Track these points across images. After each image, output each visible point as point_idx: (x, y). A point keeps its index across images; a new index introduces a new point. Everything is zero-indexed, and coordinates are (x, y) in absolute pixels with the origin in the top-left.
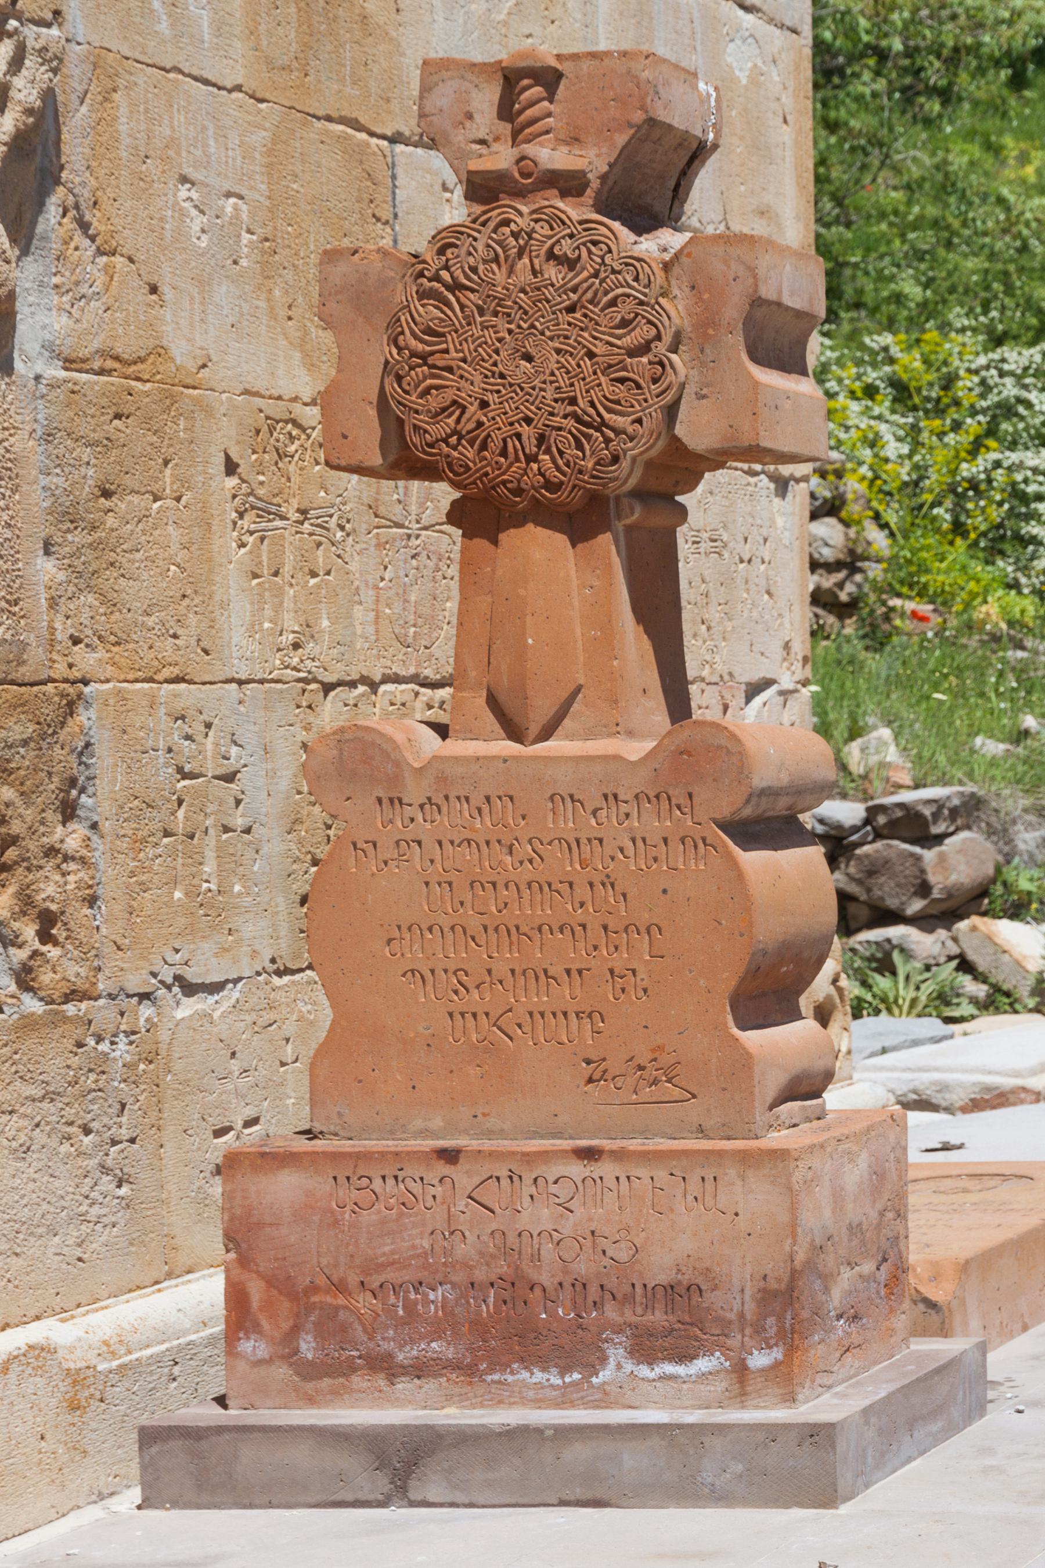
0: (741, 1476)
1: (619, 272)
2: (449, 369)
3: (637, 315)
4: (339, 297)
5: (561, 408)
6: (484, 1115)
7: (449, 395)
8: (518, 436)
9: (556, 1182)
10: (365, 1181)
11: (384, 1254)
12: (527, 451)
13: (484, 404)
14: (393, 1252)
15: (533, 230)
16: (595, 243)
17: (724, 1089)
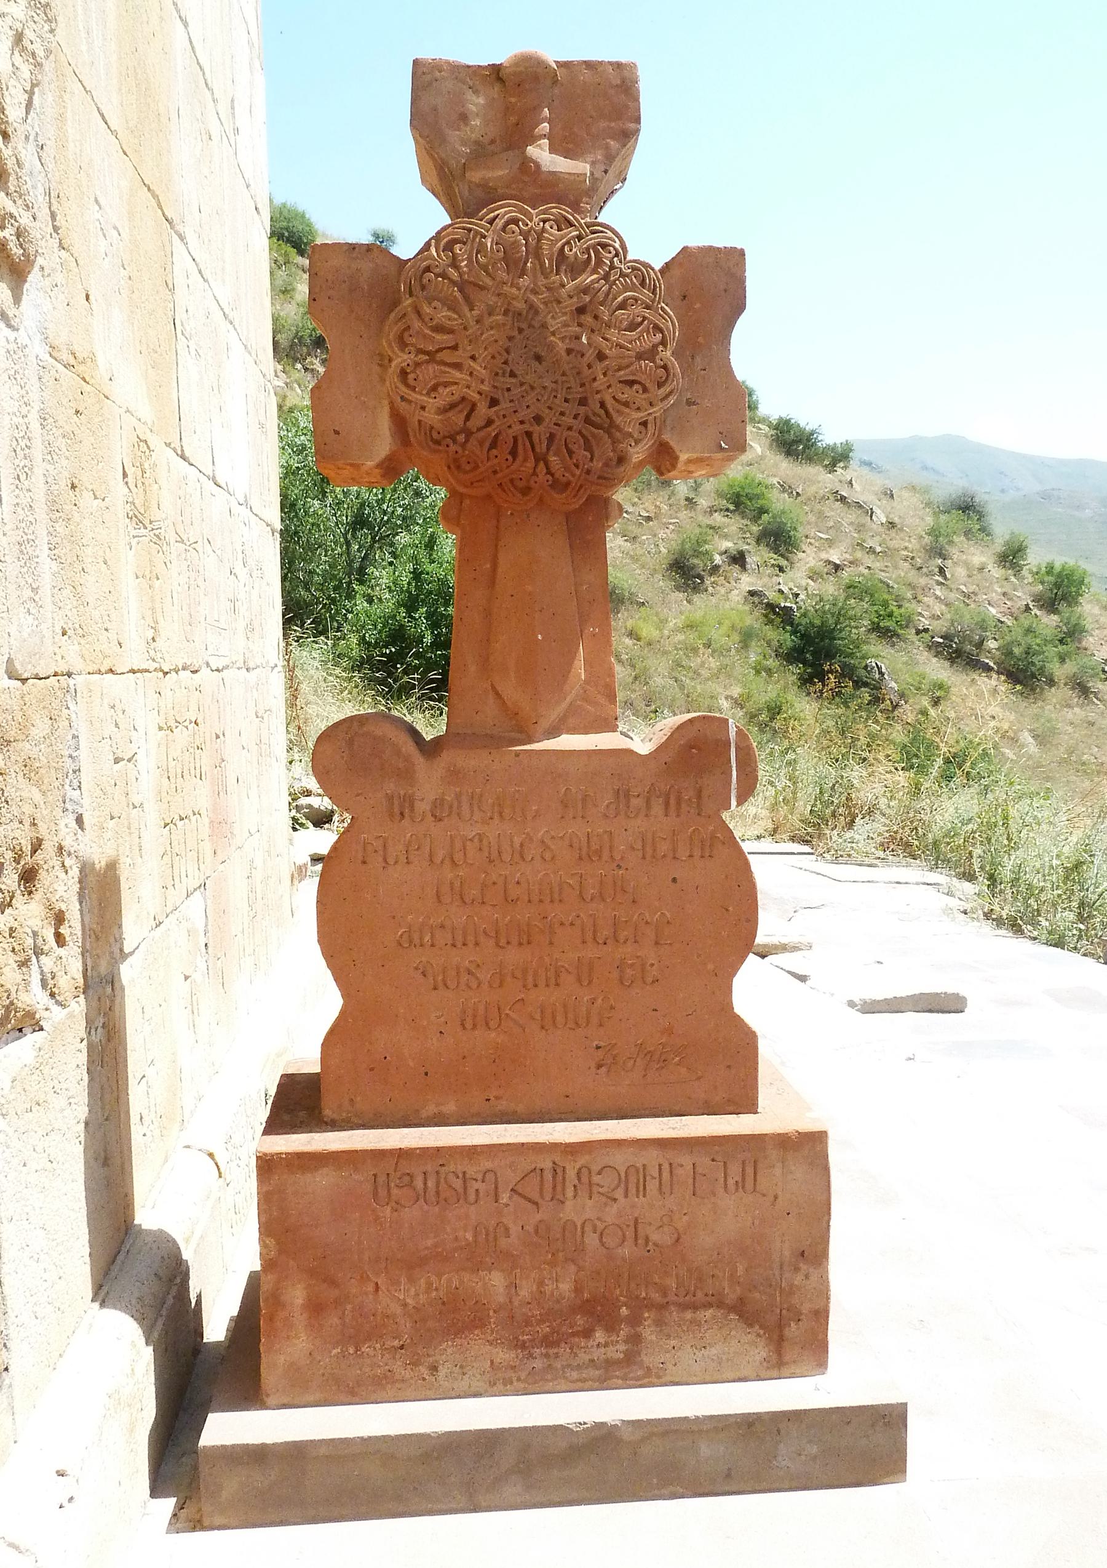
0: (816, 1457)
1: (627, 275)
2: (457, 366)
3: (644, 318)
4: (331, 292)
5: (571, 408)
6: (497, 1098)
7: (458, 392)
8: (529, 434)
9: (599, 1173)
10: (406, 1179)
11: (427, 1248)
12: (538, 450)
13: (494, 402)
14: (436, 1246)
15: (543, 230)
16: (604, 246)
17: (729, 1067)
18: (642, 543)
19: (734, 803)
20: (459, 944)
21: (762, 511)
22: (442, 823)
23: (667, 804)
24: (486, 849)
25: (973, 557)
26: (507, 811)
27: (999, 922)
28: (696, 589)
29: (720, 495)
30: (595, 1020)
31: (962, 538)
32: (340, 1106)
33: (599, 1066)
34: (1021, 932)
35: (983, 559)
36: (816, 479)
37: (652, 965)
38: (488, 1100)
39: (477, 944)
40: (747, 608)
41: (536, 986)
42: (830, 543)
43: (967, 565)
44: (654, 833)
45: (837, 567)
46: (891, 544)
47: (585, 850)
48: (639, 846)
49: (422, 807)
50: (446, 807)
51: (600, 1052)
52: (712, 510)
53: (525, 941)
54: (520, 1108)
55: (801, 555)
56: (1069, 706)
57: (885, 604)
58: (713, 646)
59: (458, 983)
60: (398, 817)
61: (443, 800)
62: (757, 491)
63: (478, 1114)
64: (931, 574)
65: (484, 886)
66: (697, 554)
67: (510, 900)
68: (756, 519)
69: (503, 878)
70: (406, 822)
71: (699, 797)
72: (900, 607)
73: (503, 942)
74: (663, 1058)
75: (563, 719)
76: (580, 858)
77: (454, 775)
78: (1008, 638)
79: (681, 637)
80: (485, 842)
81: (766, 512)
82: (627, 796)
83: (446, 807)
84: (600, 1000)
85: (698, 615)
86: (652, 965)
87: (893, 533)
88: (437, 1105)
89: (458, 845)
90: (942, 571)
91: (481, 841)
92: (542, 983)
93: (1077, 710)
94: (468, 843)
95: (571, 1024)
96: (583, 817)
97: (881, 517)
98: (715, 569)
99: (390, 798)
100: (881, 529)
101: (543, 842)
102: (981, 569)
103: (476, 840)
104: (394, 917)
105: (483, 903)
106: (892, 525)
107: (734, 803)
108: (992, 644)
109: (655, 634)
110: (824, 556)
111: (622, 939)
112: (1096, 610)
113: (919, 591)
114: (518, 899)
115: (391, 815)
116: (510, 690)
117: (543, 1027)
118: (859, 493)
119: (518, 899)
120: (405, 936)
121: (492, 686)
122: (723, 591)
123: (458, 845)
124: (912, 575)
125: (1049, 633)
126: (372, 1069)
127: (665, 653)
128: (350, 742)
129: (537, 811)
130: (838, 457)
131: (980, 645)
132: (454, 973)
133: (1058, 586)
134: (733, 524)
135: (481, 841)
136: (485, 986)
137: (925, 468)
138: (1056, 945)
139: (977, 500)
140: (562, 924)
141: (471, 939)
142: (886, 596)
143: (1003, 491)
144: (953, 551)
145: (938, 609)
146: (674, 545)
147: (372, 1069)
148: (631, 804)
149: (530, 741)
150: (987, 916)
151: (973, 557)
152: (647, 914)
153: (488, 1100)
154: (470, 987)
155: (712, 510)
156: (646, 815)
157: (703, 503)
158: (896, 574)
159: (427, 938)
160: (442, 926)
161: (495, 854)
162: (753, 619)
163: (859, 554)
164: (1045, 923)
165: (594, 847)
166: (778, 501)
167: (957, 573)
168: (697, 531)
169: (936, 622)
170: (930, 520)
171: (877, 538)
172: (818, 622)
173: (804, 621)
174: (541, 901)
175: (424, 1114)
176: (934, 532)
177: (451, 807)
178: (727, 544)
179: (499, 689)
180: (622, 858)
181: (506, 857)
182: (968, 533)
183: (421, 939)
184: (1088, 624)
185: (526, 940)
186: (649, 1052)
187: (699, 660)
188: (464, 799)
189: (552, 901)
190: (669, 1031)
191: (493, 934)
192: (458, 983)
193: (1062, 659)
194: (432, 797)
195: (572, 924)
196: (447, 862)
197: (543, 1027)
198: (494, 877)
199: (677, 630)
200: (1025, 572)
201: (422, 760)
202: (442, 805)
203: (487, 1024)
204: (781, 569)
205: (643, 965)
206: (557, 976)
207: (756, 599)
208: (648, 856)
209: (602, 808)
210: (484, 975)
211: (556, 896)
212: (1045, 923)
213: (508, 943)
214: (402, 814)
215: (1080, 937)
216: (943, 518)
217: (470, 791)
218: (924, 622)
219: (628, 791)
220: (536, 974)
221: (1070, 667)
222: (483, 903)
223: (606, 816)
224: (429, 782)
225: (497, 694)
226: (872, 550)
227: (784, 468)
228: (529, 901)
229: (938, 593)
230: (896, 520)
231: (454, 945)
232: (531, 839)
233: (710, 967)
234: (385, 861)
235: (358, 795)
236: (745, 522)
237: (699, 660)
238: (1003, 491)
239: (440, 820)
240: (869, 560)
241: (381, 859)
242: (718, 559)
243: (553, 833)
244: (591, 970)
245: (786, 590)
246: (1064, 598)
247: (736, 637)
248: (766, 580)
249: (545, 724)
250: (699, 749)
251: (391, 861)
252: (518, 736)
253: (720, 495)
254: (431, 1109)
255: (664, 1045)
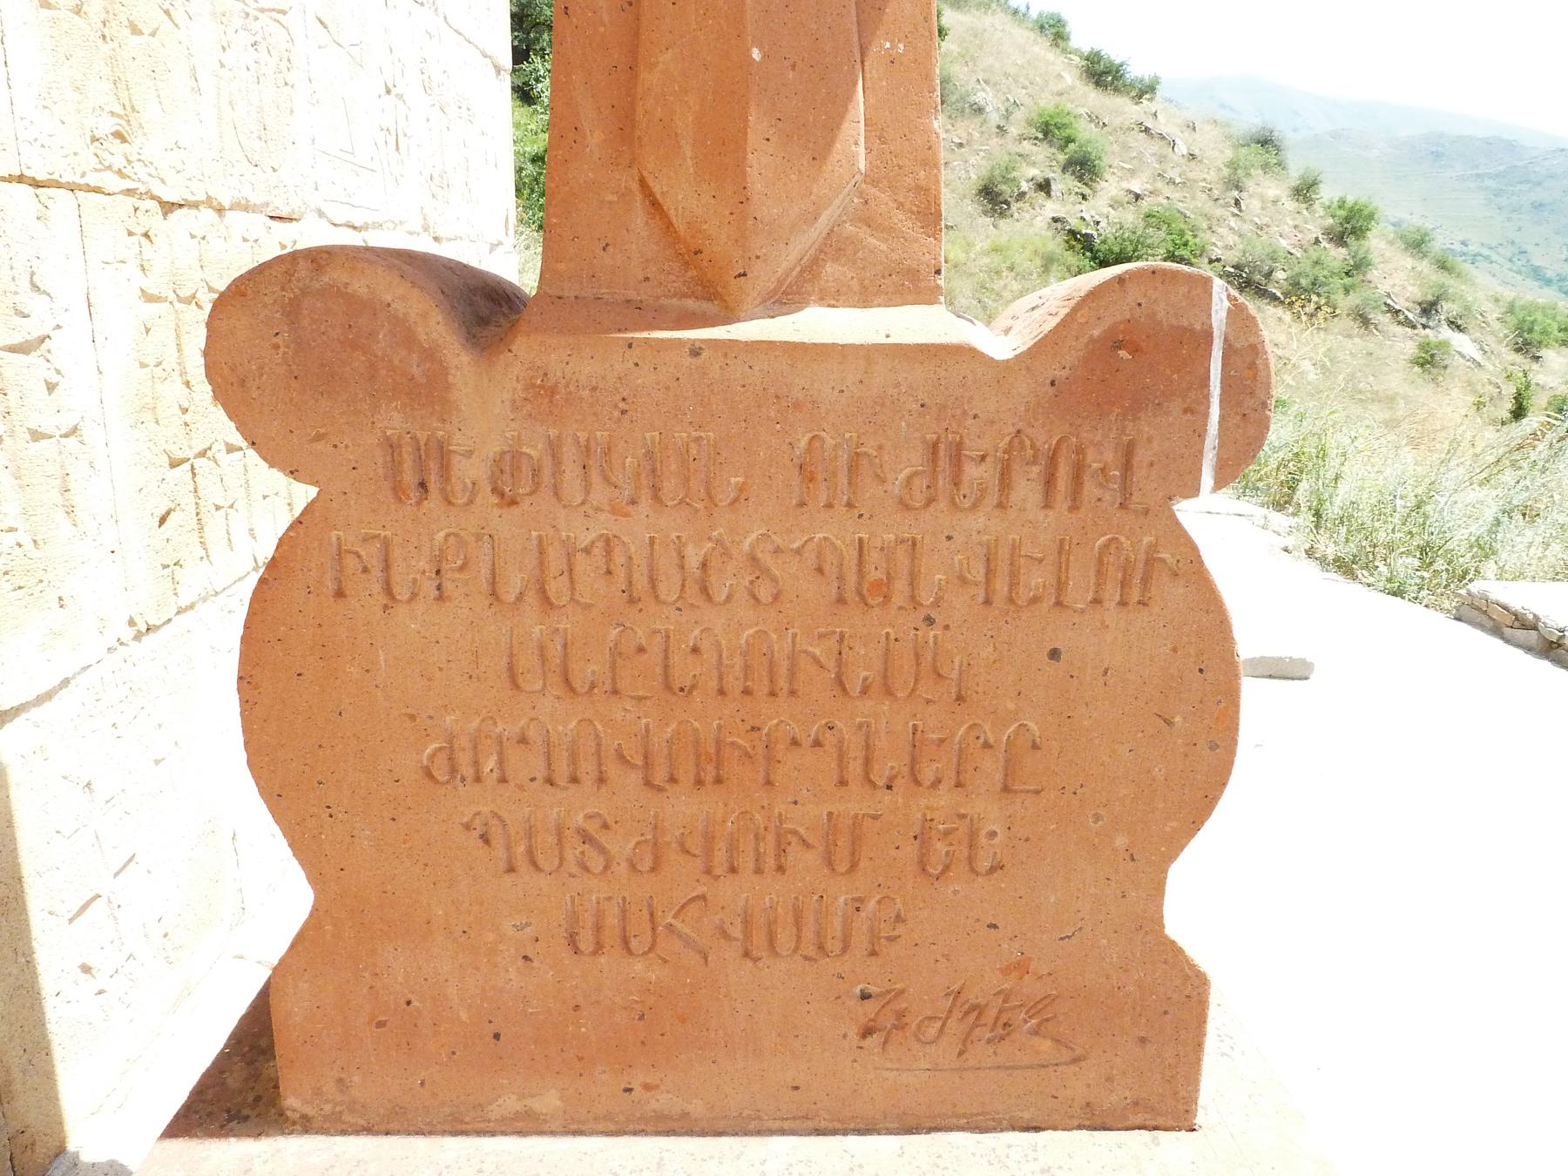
6: (647, 1087)
17: (1143, 1040)
18: (953, 169)
19: (1207, 479)
20: (562, 781)
21: (1069, 140)
22: (516, 511)
23: (1049, 482)
24: (621, 574)
25: (1267, 190)
26: (670, 486)
27: (1323, 561)
28: (1002, 214)
29: (1030, 123)
30: (860, 942)
31: (1260, 172)
32: (318, 1092)
33: (867, 1032)
34: (1355, 578)
35: (1278, 192)
36: (1121, 109)
37: (993, 834)
38: (629, 1090)
39: (601, 780)
40: (1050, 234)
41: (733, 870)
42: (1132, 173)
43: (1262, 199)
44: (1015, 547)
45: (1137, 197)
46: (1191, 175)
47: (852, 579)
48: (978, 572)
49: (471, 470)
50: (526, 470)
51: (871, 1007)
52: (1022, 138)
53: (709, 778)
54: (697, 1108)
55: (1103, 184)
56: (1349, 336)
57: (1182, 233)
58: (1018, 269)
59: (562, 859)
60: (414, 495)
61: (516, 456)
62: (1065, 121)
63: (608, 1117)
64: (1227, 205)
65: (616, 652)
66: (1006, 180)
67: (676, 686)
68: (1062, 148)
69: (658, 639)
70: (434, 501)
71: (1127, 467)
72: (1195, 236)
73: (660, 776)
74: (1004, 1018)
75: (811, 268)
76: (841, 600)
77: (544, 395)
78: (1297, 269)
79: (987, 260)
80: (619, 559)
81: (1073, 141)
82: (957, 455)
83: (526, 470)
84: (871, 905)
85: (1003, 240)
86: (993, 834)
87: (1193, 164)
88: (521, 1097)
89: (556, 560)
90: (1237, 203)
91: (608, 552)
92: (747, 862)
93: (1357, 340)
94: (580, 556)
95: (811, 951)
96: (850, 505)
97: (1182, 148)
98: (1022, 195)
99: (392, 446)
100: (1183, 161)
101: (753, 559)
102: (1275, 202)
103: (596, 551)
104: (412, 717)
105: (615, 692)
106: (1193, 156)
107: (1207, 479)
108: (1280, 275)
109: (962, 257)
110: (1125, 185)
111: (928, 775)
112: (1383, 245)
113: (1215, 222)
114: (693, 687)
115: (398, 491)
116: (684, 196)
117: (746, 954)
118: (1161, 125)
119: (693, 687)
120: (442, 759)
121: (643, 184)
122: (1027, 216)
123: (556, 560)
124: (1209, 207)
125: (1336, 265)
126: (381, 1024)
127: (971, 275)
128: (292, 311)
129: (741, 489)
130: (1145, 90)
131: (1269, 275)
132: (551, 839)
133: (1347, 220)
134: (1041, 152)
135: (608, 552)
136: (622, 869)
137: (1222, 106)
138: (1395, 594)
139: (1276, 134)
140: (795, 743)
141: (587, 768)
142: (1182, 226)
143: (1295, 130)
144: (1250, 185)
145: (1231, 239)
146: (985, 173)
147: (381, 1024)
148: (966, 478)
149: (728, 318)
150: (1310, 553)
151: (1267, 190)
152: (987, 727)
153: (629, 1090)
154: (586, 869)
155: (1022, 138)
156: (1000, 505)
157: (1013, 130)
158: (1194, 205)
159: (490, 763)
160: (523, 740)
161: (641, 583)
162: (1056, 245)
163: (1159, 185)
164: (1383, 569)
165: (874, 575)
166: (1085, 131)
167: (1251, 204)
168: (1006, 158)
169: (1229, 253)
170: (1229, 154)
171: (1178, 170)
172: (1116, 249)
173: (1103, 248)
174: (747, 692)
175: (495, 1111)
176: (1233, 165)
177: (536, 472)
178: (1034, 172)
179: (656, 189)
180: (936, 604)
181: (669, 590)
182: (1265, 167)
183: (476, 763)
184: (1374, 257)
185: (710, 767)
186: (974, 1008)
187: (1002, 283)
188: (569, 453)
189: (773, 694)
190: (1020, 968)
191: (639, 761)
192: (562, 859)
193: (1347, 291)
194: (494, 448)
195: (817, 743)
196: (531, 598)
197: (746, 954)
198: (641, 635)
199: (987, 253)
200: (1317, 206)
201: (465, 358)
202: (516, 470)
203: (626, 942)
204: (1084, 197)
205: (973, 836)
206: (781, 851)
207: (1059, 225)
208: (999, 599)
209: (896, 488)
210: (620, 846)
211: (782, 683)
212: (1383, 569)
213: (673, 780)
214: (422, 485)
215: (1421, 589)
216: (1244, 150)
217: (583, 436)
218: (1216, 252)
219: (959, 446)
220: (733, 847)
221: (1354, 299)
222: (615, 692)
223: (904, 505)
224: (485, 408)
225: (655, 204)
226: (1172, 182)
227: (1092, 98)
228: (721, 692)
229: (1232, 224)
230: (1197, 152)
231: (550, 781)
232: (726, 554)
233: (1121, 841)
234: (388, 590)
235: (319, 438)
236: (1053, 150)
237: (1002, 283)
238: (1295, 130)
239: (513, 503)
240: (1168, 191)
241: (377, 588)
242: (1025, 186)
243: (778, 540)
244: (856, 841)
245: (1087, 217)
246: (1353, 232)
247: (1038, 262)
248: (1069, 207)
249: (763, 278)
250: (1135, 350)
251: (402, 593)
252: (705, 306)
253: (1030, 123)
254: (510, 1104)
255: (1006, 996)
